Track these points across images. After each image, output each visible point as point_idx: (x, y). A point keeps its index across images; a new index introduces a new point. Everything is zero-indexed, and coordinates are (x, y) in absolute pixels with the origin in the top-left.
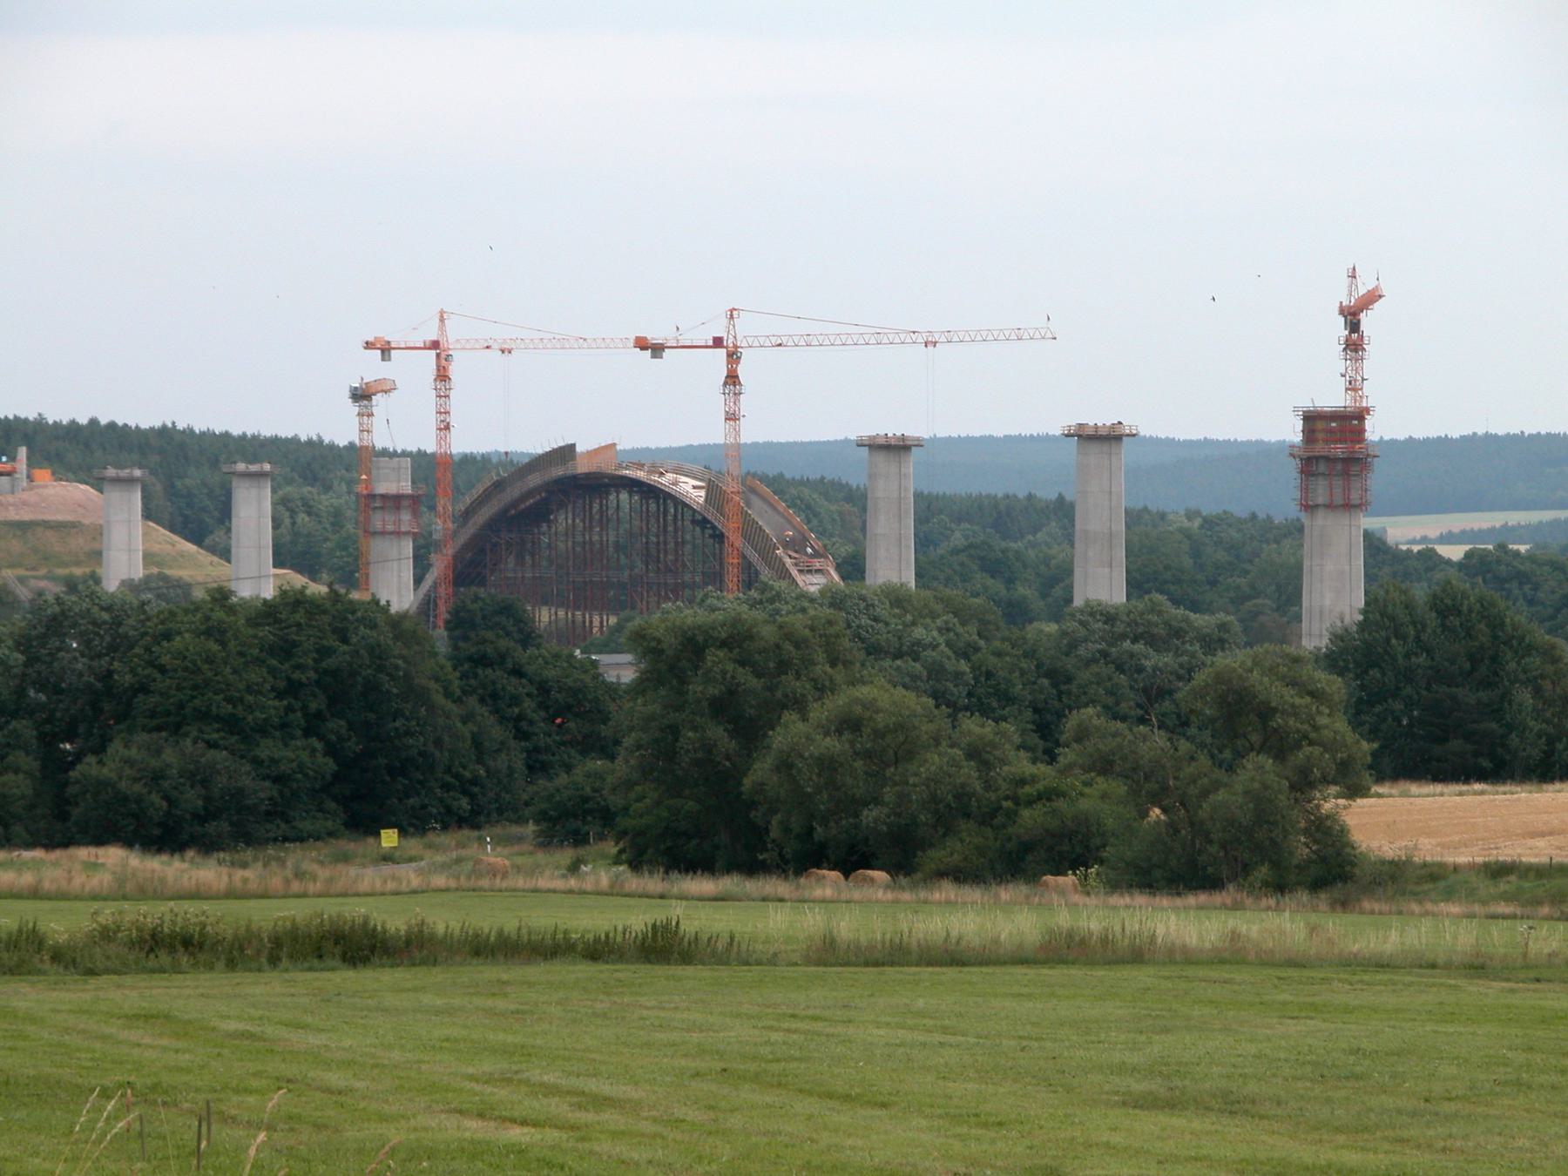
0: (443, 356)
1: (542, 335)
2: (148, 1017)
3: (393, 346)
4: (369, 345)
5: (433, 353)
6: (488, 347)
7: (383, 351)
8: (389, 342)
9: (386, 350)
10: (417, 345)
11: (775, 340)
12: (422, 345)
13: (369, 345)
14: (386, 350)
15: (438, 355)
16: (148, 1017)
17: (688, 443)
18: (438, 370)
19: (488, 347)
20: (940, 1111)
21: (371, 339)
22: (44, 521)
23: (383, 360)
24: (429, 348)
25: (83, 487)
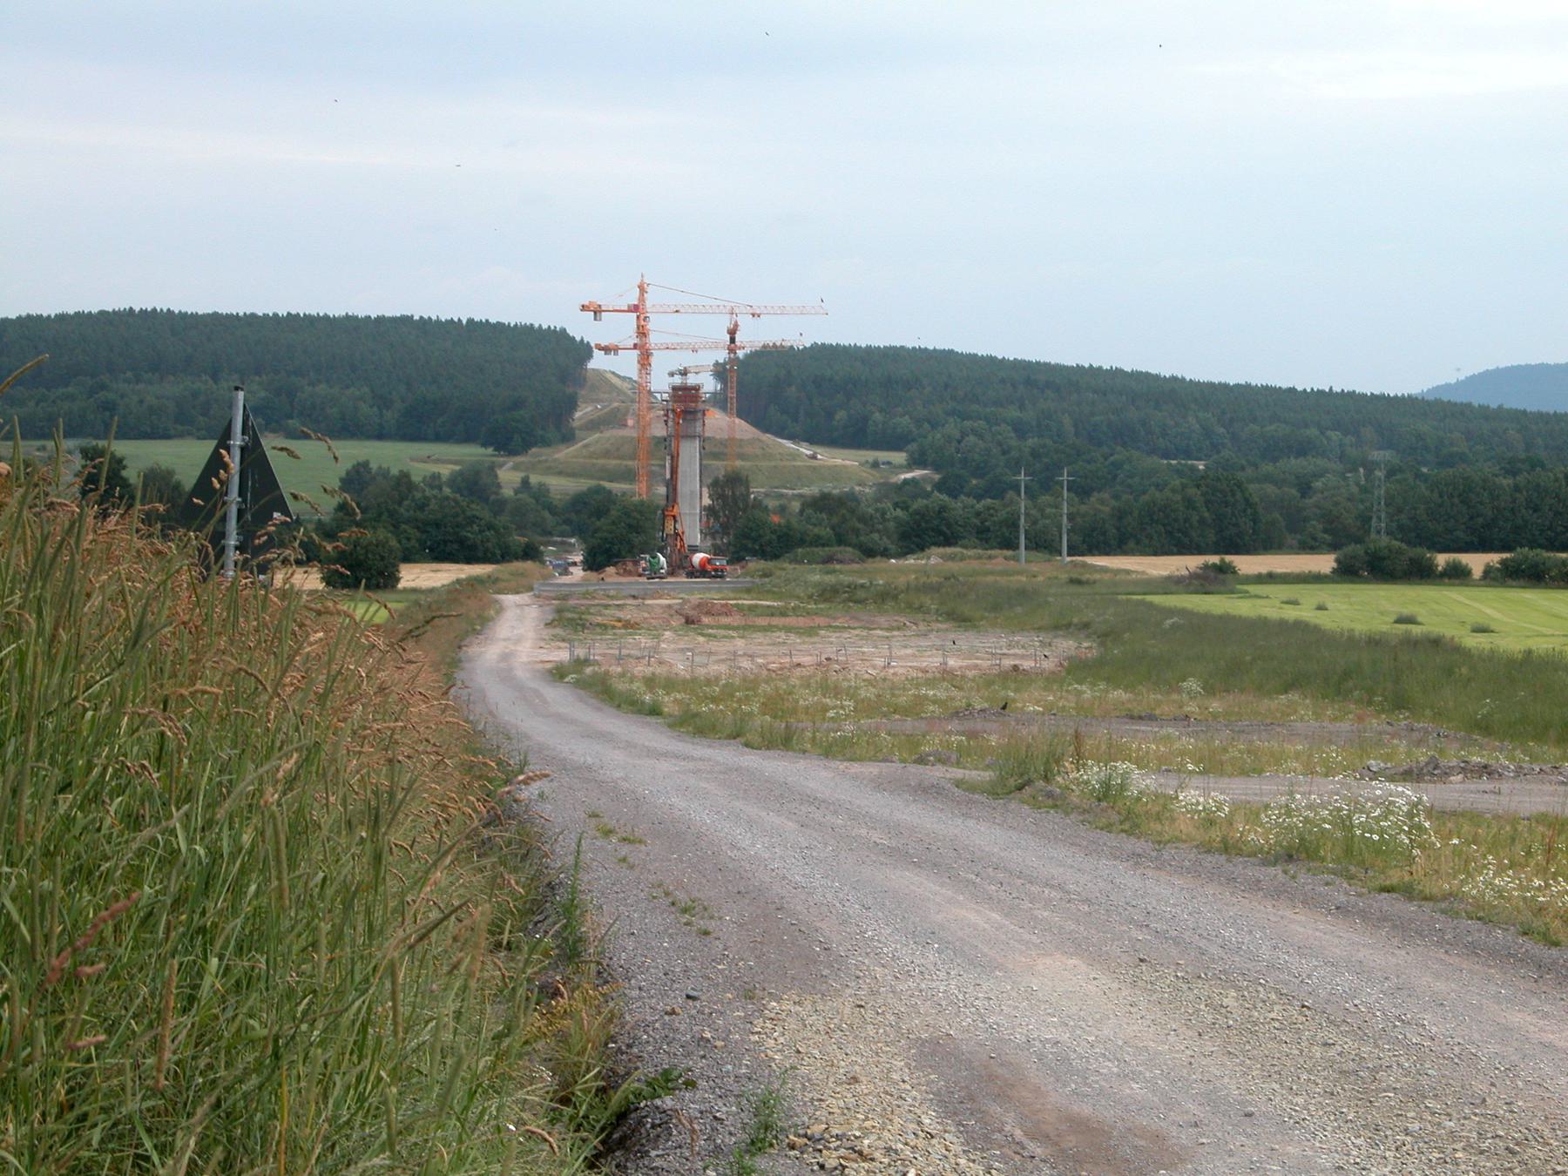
0: (642, 317)
1: (718, 302)
2: (282, 449)
3: (603, 308)
4: (584, 308)
5: (634, 315)
6: (677, 311)
7: (595, 313)
8: (600, 306)
9: (597, 312)
10: (623, 308)
11: (665, 346)
12: (626, 308)
13: (584, 308)
14: (597, 312)
15: (638, 317)
16: (282, 449)
17: (1485, 369)
18: (638, 328)
19: (677, 311)
20: (1035, 889)
21: (587, 303)
22: (962, 621)
23: (595, 319)
24: (632, 312)
25: (768, 435)
